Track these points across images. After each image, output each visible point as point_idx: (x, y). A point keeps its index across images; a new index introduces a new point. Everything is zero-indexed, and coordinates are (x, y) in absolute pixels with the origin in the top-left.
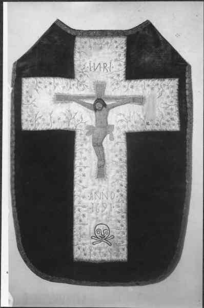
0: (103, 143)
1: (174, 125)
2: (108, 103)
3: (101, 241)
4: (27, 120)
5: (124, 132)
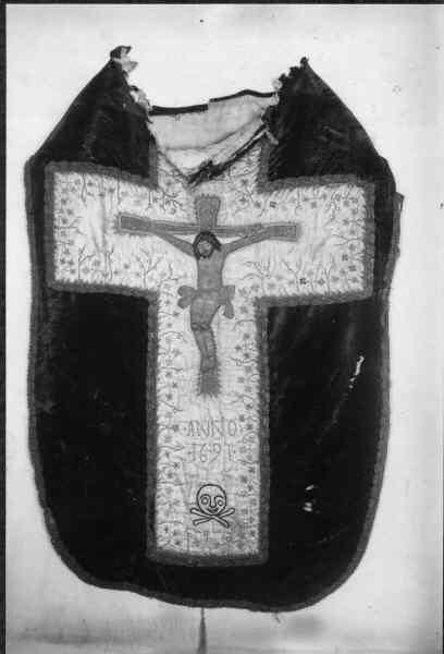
0: (213, 325)
1: (355, 280)
2: (223, 241)
3: (209, 520)
4: (63, 262)
5: (254, 300)
